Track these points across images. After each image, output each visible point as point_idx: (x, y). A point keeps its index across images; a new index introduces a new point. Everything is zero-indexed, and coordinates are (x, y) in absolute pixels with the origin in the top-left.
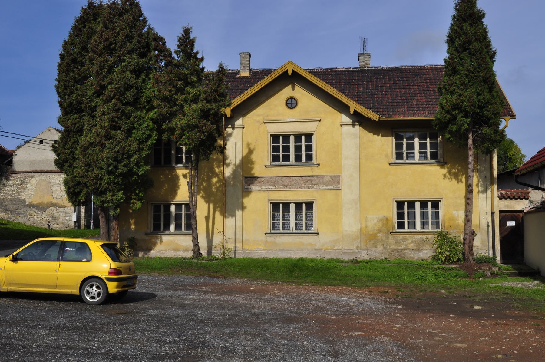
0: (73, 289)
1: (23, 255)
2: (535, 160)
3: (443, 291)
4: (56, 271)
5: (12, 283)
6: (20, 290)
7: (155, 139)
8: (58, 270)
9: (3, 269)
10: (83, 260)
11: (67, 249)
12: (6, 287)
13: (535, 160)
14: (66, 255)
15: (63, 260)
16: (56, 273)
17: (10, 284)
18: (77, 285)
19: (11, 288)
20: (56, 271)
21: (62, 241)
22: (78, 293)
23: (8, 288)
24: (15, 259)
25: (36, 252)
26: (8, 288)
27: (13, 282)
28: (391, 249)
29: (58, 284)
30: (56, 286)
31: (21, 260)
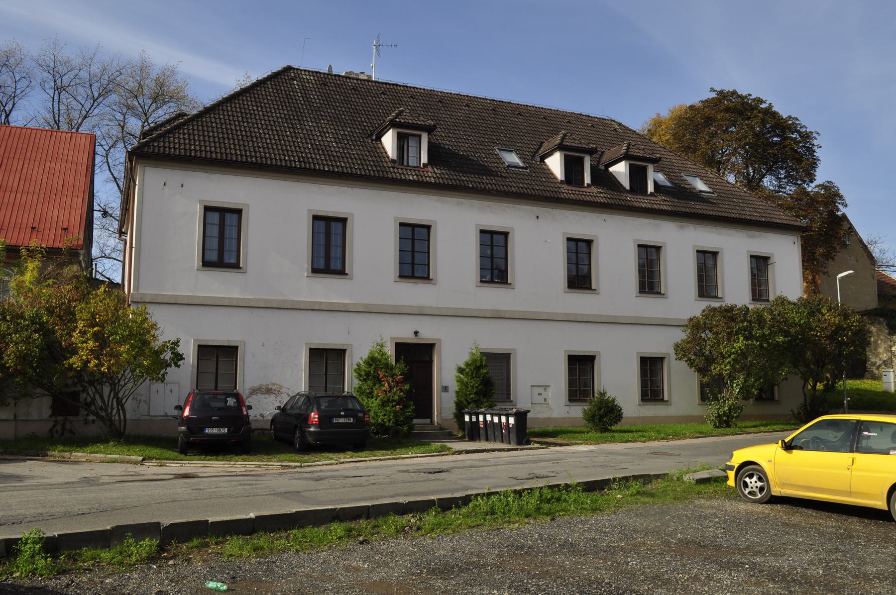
0: (876, 499)
1: (804, 442)
2: (127, 475)
3: (775, 139)
4: (849, 469)
5: (787, 484)
6: (798, 495)
7: (74, 351)
8: (850, 467)
9: (773, 461)
10: (891, 453)
11: (865, 433)
12: (779, 489)
13: (127, 475)
14: (864, 443)
15: (858, 451)
16: (848, 472)
17: (784, 484)
18: (883, 493)
19: (785, 490)
20: (849, 469)
21: (858, 421)
22: (886, 508)
23: (782, 490)
24: (788, 447)
25: (830, 435)
26: (782, 490)
27: (788, 482)
28: (181, 110)
29: (852, 491)
30: (850, 494)
31: (801, 448)
